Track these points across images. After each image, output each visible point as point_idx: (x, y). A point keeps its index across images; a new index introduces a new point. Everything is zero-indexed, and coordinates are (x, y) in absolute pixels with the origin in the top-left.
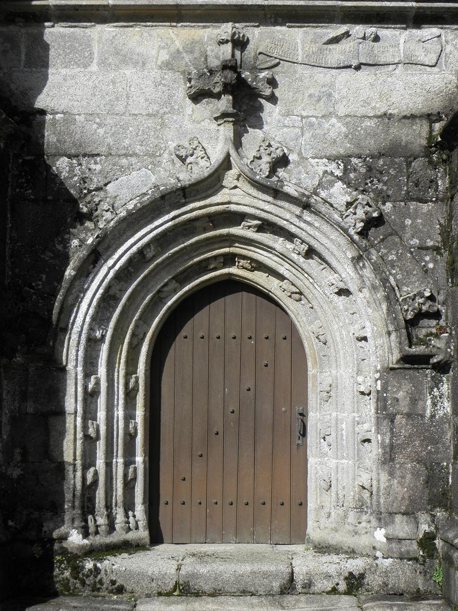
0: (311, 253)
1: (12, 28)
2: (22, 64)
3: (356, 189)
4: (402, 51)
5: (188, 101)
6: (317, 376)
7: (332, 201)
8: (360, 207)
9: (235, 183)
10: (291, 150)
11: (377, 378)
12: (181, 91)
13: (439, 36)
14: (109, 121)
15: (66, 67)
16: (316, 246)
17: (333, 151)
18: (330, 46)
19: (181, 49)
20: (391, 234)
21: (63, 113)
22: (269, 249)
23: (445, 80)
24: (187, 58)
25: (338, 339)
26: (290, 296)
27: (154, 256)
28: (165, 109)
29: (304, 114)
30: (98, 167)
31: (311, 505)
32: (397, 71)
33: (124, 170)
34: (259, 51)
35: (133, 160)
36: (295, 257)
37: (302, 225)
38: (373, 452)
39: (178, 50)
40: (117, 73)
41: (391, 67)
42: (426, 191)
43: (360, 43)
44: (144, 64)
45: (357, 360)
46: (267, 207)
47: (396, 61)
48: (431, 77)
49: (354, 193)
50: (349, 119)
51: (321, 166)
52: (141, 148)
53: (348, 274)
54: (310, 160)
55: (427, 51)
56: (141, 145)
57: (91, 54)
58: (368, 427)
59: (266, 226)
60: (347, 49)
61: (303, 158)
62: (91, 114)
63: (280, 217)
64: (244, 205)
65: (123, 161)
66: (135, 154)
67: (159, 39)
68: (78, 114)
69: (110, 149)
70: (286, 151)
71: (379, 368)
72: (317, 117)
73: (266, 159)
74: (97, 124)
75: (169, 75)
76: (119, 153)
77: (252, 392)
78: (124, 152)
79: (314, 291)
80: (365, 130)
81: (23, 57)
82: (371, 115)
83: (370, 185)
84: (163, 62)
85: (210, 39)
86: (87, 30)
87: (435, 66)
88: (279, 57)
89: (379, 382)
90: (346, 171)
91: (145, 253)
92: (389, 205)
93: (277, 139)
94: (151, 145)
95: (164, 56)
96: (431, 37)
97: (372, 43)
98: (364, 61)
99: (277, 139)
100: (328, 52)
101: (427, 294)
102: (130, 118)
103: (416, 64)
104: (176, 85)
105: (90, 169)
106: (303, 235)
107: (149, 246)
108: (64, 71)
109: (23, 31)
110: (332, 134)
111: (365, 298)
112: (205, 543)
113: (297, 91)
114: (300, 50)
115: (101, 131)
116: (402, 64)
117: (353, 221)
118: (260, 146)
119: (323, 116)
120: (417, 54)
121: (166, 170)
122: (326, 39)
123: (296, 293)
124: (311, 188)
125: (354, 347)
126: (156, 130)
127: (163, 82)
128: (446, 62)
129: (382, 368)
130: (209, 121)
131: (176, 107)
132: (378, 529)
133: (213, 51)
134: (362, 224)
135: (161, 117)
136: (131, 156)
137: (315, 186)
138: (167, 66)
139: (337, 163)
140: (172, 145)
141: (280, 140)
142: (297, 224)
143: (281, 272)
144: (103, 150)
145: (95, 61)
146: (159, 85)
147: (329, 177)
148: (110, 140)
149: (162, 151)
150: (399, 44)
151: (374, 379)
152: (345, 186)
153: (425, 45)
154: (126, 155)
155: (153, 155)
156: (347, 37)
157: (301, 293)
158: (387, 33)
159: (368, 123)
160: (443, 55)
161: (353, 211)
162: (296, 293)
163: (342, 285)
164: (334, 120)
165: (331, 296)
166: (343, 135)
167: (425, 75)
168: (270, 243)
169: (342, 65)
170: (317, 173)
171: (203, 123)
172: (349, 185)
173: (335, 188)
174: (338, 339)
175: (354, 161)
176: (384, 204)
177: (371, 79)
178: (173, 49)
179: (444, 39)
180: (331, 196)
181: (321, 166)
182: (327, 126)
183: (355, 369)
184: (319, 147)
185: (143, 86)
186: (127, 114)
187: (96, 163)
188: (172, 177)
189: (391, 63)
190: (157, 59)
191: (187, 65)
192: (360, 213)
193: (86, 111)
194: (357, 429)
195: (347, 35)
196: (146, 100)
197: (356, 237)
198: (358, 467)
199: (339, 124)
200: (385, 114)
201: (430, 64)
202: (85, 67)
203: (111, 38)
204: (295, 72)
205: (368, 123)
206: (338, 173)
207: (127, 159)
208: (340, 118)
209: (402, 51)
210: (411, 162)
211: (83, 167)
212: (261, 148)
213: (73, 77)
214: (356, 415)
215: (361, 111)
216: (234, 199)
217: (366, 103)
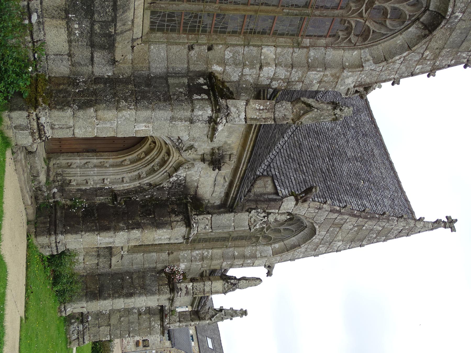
53: (146, 181)
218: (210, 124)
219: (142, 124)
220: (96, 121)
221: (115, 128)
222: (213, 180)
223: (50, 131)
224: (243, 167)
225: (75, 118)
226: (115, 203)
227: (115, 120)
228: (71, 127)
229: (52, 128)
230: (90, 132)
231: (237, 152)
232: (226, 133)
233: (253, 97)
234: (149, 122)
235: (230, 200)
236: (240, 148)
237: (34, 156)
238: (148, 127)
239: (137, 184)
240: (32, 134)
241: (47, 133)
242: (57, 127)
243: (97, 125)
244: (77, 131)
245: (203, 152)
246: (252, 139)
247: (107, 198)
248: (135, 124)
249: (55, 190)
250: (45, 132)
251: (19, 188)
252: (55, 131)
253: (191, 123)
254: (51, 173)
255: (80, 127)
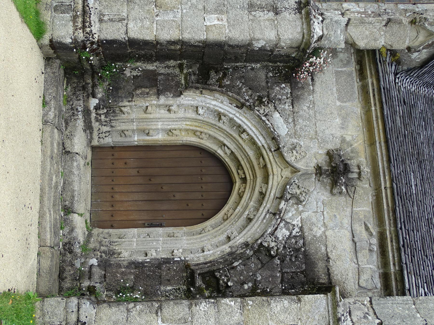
0: (250, 220)
1: (354, 64)
2: (337, 69)
3: (285, 243)
4: (365, 266)
5: (325, 151)
6: (182, 230)
7: (279, 230)
8: (276, 244)
9: (284, 177)
10: (304, 206)
11: (181, 258)
12: (330, 146)
13: (376, 288)
14: (311, 112)
15: (337, 90)
16: (253, 222)
17: (306, 229)
18: (363, 226)
19: (353, 147)
20: (262, 263)
21: (313, 89)
22: (250, 198)
23: (351, 292)
24: (349, 149)
25: (203, 239)
26: (225, 214)
27: (242, 138)
28: (320, 139)
29: (325, 213)
30: (287, 107)
31: (111, 231)
32: (354, 264)
33: (286, 121)
34: (356, 187)
35: (292, 125)
36: (246, 213)
37: (264, 214)
38: (140, 258)
39: (352, 145)
40: (337, 115)
41: (355, 260)
42: (287, 283)
43: (367, 242)
44: (343, 128)
45: (191, 249)
46: (272, 194)
47: (359, 263)
48: (352, 284)
49: (284, 242)
50: (324, 237)
51: (297, 222)
52: (298, 128)
53: (239, 240)
54: (300, 217)
55: (367, 281)
56: (300, 128)
57: (345, 102)
58: (153, 254)
59: (262, 195)
60: (362, 235)
61: (301, 213)
62: (314, 103)
63: (267, 201)
64: (273, 182)
65: (291, 119)
66: (295, 125)
67: (357, 136)
68: (313, 97)
69: (297, 113)
70: (304, 203)
71: (187, 259)
72: (324, 220)
73: (298, 192)
74: (309, 106)
75: (338, 141)
76: (295, 117)
77: (173, 198)
78: (296, 120)
79: (228, 225)
80: (319, 247)
81: (340, 69)
82: (328, 250)
83: (289, 250)
84: (345, 138)
85: (360, 161)
86: (357, 100)
87: (359, 285)
88: (354, 198)
89: (179, 259)
90: (295, 237)
91: (244, 133)
92: (279, 262)
93: (310, 198)
94: (300, 133)
95: (348, 138)
96: (375, 283)
97: (368, 248)
98: (357, 244)
99: (310, 198)
100: (360, 224)
101: (230, 284)
102: (314, 122)
103: (359, 275)
104: (334, 145)
105: (285, 103)
106: (258, 215)
107: (248, 135)
108: (335, 89)
109: (354, 69)
110: (315, 229)
111: (226, 249)
112: (92, 176)
113: (337, 209)
114: (360, 209)
115: (305, 108)
116: (358, 267)
117: (268, 240)
118: (305, 188)
119: (324, 223)
120: (365, 275)
121: (288, 141)
122: (367, 223)
123: (227, 217)
124: (284, 218)
125: (198, 247)
126: (309, 135)
127: (335, 138)
128: (362, 292)
129: (187, 261)
130: (316, 162)
131: (322, 145)
132: (97, 261)
133: (354, 163)
134: (266, 246)
135: (315, 138)
136: (294, 123)
137: (286, 220)
138: (343, 140)
139: (299, 232)
140: (302, 143)
141: (309, 200)
142: (264, 211)
143: (238, 207)
144: (296, 109)
145: (342, 104)
146: (333, 136)
147: (291, 227)
148: (301, 113)
149: (298, 139)
150: (369, 264)
151: (180, 256)
152: (287, 237)
153: (370, 280)
154: (294, 120)
155: (295, 134)
156: (369, 235)
157: (227, 219)
158: (375, 257)
159: (323, 248)
160: (366, 291)
161: (273, 240)
162: (227, 217)
163: (232, 238)
164: (323, 229)
165: (226, 233)
166: (315, 234)
167: (353, 280)
168: (253, 199)
169: (354, 232)
170: (293, 221)
171: (315, 159)
172: (288, 239)
173: (286, 231)
174: (203, 239)
175: (301, 242)
176: (279, 259)
177: (348, 250)
178: (352, 142)
179: (375, 291)
180: (281, 229)
181: (297, 222)
182: (319, 225)
183: (186, 248)
184: (307, 222)
185: (331, 128)
186: (316, 121)
187: (289, 106)
188: (285, 144)
189: (358, 260)
190: (346, 135)
191: (345, 150)
192: (273, 244)
193: (315, 100)
194: (153, 250)
195: (371, 234)
196: (324, 130)
197: (259, 241)
198: (131, 251)
199: (321, 232)
200: (329, 258)
201: (360, 283)
202: (339, 99)
203: (355, 111)
204: (347, 207)
205: (323, 248)
206: (294, 233)
207: (292, 121)
208: (325, 233)
209: (365, 266)
210: (303, 274)
211: (286, 100)
212: (304, 189)
213: (332, 94)
214: (161, 249)
215: (329, 246)
216: (275, 177)
217: (334, 247)
218: (300, 13)
219: (213, 15)
220: (155, 9)
221: (180, 23)
222: (348, 235)
223: (98, 25)
224: (385, 183)
225: (130, 3)
226: (192, 289)
227: (179, 9)
228: (124, 20)
229: (101, 21)
230: (148, 29)
231: (366, 158)
232: (337, 120)
233: (354, 53)
234: (221, 12)
235: (394, 283)
236: (368, 150)
237: (72, 158)
238: (222, 20)
239: (226, 248)
240: (74, 19)
241: (93, 26)
242: (106, 18)
243: (157, 15)
244: (131, 25)
245: (316, 161)
246: (377, 117)
247: (179, 289)
248: (205, 15)
249: (94, 261)
250: (90, 23)
251: (39, 187)
252: (104, 25)
253: (277, 14)
254: (93, 239)
255: (135, 19)
